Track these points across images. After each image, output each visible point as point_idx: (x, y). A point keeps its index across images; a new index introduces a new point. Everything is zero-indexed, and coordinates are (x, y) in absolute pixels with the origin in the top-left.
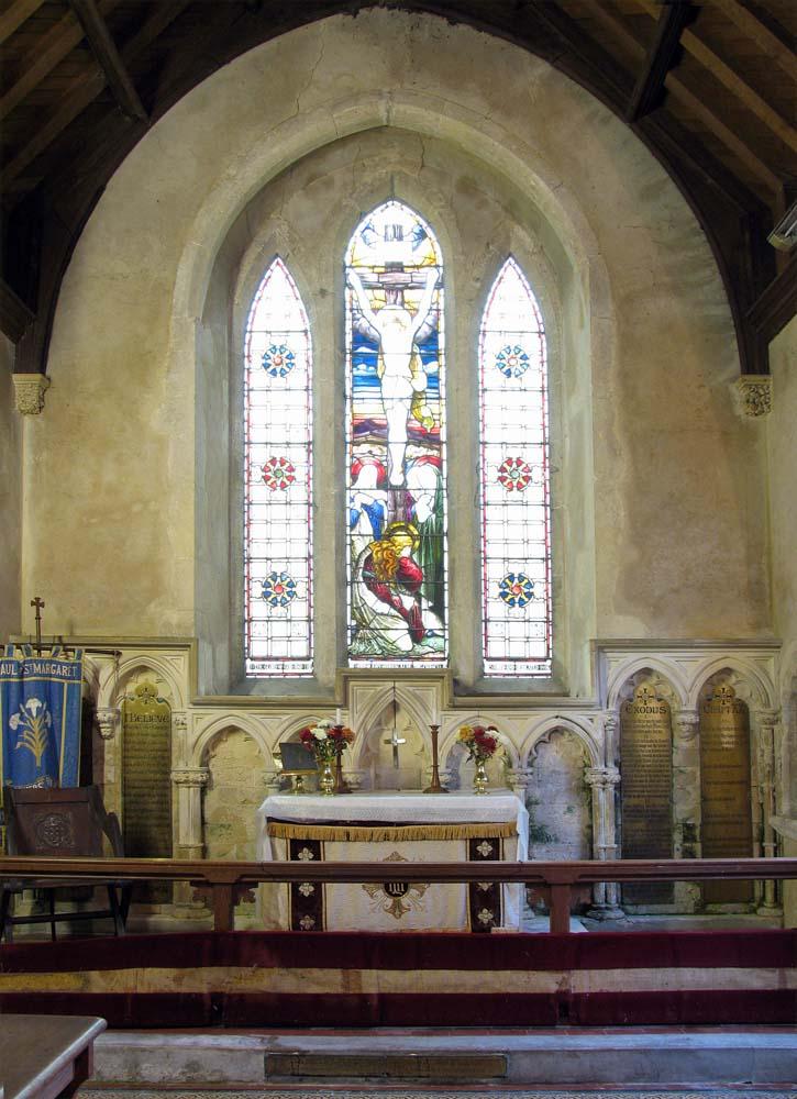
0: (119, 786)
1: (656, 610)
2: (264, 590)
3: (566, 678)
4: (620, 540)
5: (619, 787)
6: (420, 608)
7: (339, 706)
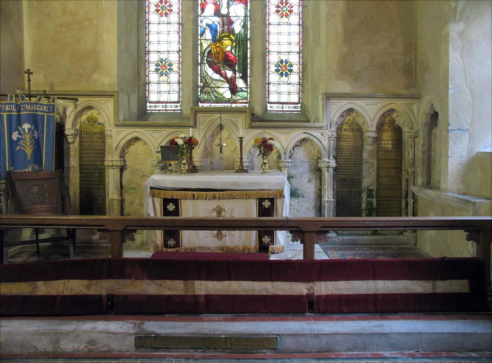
0: (78, 169)
1: (356, 77)
2: (156, 67)
3: (308, 113)
4: (339, 41)
5: (335, 169)
6: (235, 77)
7: (191, 127)
